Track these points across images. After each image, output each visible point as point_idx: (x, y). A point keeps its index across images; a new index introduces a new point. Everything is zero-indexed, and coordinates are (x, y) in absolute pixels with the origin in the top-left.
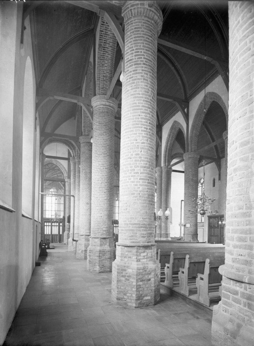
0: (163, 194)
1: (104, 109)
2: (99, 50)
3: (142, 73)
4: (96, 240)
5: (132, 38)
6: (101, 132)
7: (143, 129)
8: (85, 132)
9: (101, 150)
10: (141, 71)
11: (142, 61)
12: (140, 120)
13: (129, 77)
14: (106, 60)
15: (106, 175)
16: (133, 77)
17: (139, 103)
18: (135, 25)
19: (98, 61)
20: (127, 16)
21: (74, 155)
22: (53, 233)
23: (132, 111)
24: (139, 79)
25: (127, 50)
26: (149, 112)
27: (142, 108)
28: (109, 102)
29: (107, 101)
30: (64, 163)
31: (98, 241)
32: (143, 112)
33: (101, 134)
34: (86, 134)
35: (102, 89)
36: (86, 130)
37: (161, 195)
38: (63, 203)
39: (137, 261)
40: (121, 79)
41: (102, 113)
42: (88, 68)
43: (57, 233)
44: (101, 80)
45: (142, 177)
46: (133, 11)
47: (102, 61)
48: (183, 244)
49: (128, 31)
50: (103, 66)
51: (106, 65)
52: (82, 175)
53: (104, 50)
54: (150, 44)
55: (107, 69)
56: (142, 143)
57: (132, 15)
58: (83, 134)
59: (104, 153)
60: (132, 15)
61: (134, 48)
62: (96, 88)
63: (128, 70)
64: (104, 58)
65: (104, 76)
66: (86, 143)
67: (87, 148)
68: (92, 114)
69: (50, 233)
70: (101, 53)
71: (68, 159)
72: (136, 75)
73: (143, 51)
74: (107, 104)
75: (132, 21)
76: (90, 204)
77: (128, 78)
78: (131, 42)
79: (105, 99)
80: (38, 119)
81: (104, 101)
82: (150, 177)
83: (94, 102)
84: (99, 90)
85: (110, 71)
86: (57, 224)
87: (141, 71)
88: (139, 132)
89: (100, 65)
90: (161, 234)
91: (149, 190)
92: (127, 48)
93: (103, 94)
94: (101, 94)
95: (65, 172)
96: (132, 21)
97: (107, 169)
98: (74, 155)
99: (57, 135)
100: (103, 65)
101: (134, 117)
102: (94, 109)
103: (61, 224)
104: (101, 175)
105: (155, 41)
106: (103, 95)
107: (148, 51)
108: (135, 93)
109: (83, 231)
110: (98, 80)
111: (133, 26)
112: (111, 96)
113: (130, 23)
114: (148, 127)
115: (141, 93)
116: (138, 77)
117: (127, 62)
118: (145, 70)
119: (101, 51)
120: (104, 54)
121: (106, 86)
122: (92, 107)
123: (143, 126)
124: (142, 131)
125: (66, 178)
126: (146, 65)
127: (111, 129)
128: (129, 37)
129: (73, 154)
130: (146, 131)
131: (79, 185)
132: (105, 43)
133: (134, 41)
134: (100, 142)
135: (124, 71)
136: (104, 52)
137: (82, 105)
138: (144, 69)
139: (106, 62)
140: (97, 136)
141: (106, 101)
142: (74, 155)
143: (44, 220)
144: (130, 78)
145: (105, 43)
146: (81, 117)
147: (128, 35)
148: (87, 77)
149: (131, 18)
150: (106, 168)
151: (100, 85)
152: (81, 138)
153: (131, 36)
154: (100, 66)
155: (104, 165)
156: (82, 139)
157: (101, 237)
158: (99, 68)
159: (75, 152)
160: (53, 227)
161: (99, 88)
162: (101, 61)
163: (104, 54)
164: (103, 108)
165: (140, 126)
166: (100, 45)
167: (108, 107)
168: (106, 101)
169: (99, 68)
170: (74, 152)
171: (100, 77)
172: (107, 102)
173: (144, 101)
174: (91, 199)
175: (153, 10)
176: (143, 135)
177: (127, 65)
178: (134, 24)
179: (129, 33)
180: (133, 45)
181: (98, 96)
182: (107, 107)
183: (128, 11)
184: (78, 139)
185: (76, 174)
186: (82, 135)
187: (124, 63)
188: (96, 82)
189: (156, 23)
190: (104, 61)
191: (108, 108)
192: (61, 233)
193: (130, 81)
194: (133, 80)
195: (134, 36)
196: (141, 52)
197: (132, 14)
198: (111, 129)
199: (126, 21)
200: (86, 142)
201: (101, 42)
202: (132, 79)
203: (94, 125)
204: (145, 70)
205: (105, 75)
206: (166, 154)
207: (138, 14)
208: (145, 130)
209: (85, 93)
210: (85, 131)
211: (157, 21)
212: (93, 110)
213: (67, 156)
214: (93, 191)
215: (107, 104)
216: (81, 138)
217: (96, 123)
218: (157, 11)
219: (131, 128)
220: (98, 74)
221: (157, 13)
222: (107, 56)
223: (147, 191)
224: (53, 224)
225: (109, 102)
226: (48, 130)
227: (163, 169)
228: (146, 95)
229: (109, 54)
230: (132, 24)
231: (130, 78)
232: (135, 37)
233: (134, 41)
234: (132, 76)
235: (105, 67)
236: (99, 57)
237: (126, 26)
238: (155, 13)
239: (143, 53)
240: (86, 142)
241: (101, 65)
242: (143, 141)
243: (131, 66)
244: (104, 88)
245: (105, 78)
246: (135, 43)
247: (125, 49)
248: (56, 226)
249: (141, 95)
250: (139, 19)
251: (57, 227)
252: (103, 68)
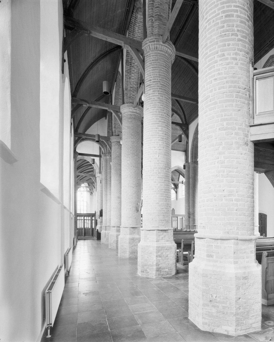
0: (190, 188)
1: (131, 116)
2: (127, 65)
3: (158, 96)
4: (126, 229)
5: (150, 68)
6: (129, 136)
7: (160, 139)
8: (115, 132)
9: (129, 151)
10: (157, 94)
11: (158, 87)
12: (157, 132)
13: (149, 98)
14: (133, 73)
15: (134, 172)
16: (151, 99)
17: (156, 119)
18: (152, 58)
19: (126, 74)
20: (146, 50)
21: (105, 152)
22: (85, 227)
23: (236, 17)
24: (156, 100)
25: (147, 77)
26: (165, 126)
27: (159, 122)
28: (136, 110)
29: (134, 108)
30: (97, 159)
31: (128, 230)
32: (160, 126)
33: (129, 137)
34: (117, 134)
35: (130, 98)
36: (116, 131)
37: (189, 189)
38: (121, 98)
39: (157, 241)
40: (143, 99)
41: (130, 119)
42: (118, 76)
43: (90, 227)
44: (129, 91)
45: (160, 176)
46: (150, 46)
47: (129, 74)
48: (64, 180)
49: (147, 62)
50: (130, 79)
51: (132, 78)
52: (113, 171)
53: (130, 65)
54: (165, 73)
55: (134, 81)
56: (159, 150)
57: (150, 49)
58: (114, 134)
59: (132, 153)
60: (150, 49)
61: (152, 76)
62: (125, 97)
63: (148, 93)
64: (131, 72)
65: (131, 87)
66: (116, 143)
67: (117, 147)
68: (121, 120)
69: (82, 227)
70: (128, 67)
71: (100, 156)
72: (154, 97)
73: (159, 78)
74: (134, 111)
75: (150, 54)
76: (120, 198)
77: (148, 99)
78: (150, 71)
79: (132, 107)
80: (72, 124)
81: (131, 109)
82: (166, 176)
83: (123, 109)
84: (127, 99)
85: (136, 83)
86: (90, 218)
87: (157, 94)
88: (157, 141)
89: (127, 77)
90: (189, 226)
91: (165, 186)
92: (147, 76)
93: (131, 103)
94: (129, 103)
95: (97, 167)
96: (150, 54)
97: (134, 167)
98: (106, 152)
99: (88, 135)
100: (130, 78)
101: (153, 130)
102: (123, 116)
103: (93, 218)
104: (130, 172)
105: (169, 70)
106: (130, 104)
107: (164, 78)
108: (153, 111)
109: (114, 222)
110: (125, 90)
111: (151, 58)
112: (137, 104)
113: (148, 56)
114: (164, 137)
115: (158, 111)
116: (156, 99)
117: (147, 86)
118: (161, 94)
119: (129, 66)
120: (131, 68)
121: (132, 96)
122: (121, 113)
123: (160, 137)
124: (159, 140)
125: (98, 173)
126: (162, 89)
127: (138, 132)
128: (148, 67)
129: (105, 152)
130: (162, 140)
131: (111, 181)
132: (131, 59)
133: (152, 70)
134: (128, 144)
135: (145, 93)
136: (131, 66)
137: (112, 111)
138: (160, 92)
139: (133, 75)
140: (126, 139)
141: (133, 109)
142: (106, 152)
143: (77, 215)
144: (149, 99)
145: (131, 59)
146: (112, 120)
147: (148, 65)
148: (116, 84)
149: (149, 52)
150: (133, 167)
151: (127, 94)
152: (112, 138)
153: (150, 66)
154: (127, 79)
155: (132, 164)
156: (113, 139)
157: (130, 227)
158: (126, 80)
159: (107, 150)
160: (85, 221)
161: (127, 97)
162: (129, 74)
163: (131, 68)
164: (131, 114)
165: (157, 136)
166: (127, 61)
167: (135, 114)
168: (133, 109)
169: (126, 80)
170: (105, 150)
171: (127, 88)
172: (135, 109)
173: (160, 117)
174: (121, 194)
175: (167, 45)
176: (160, 143)
177: (147, 89)
178: (151, 57)
179: (148, 64)
180: (152, 74)
181: (126, 105)
182: (134, 113)
183: (147, 46)
184: (109, 139)
185: (108, 170)
186: (113, 135)
187: (145, 86)
188: (125, 92)
189: (169, 55)
190: (130, 74)
191: (135, 115)
192: (93, 227)
193: (149, 101)
194: (151, 101)
195: (152, 66)
196: (158, 79)
197: (150, 48)
198: (138, 132)
199: (146, 54)
200: (117, 142)
201: (128, 58)
202: (150, 100)
203: (123, 129)
204: (161, 94)
205: (132, 86)
206: (193, 151)
207: (154, 49)
208: (162, 139)
209: (115, 98)
210: (115, 131)
211: (170, 54)
212: (122, 116)
213: (98, 154)
214: (123, 187)
215: (134, 111)
216: (112, 138)
217: (125, 127)
218: (170, 46)
219: (150, 138)
220: (126, 85)
221: (170, 47)
222: (133, 70)
223: (164, 187)
224: (85, 218)
225: (136, 110)
226: (80, 130)
227: (190, 164)
228: (162, 112)
229: (135, 69)
230: (150, 56)
231: (149, 99)
232: (152, 68)
233: (152, 70)
234: (150, 98)
235: (132, 79)
236: (127, 71)
237: (145, 58)
238: (168, 48)
239: (159, 80)
240: (117, 142)
241: (128, 78)
242: (160, 148)
243: (150, 90)
244: (131, 98)
245: (132, 89)
246: (152, 72)
247: (145, 76)
248: (89, 220)
249: (158, 113)
250: (155, 53)
251: (90, 221)
252: (130, 80)
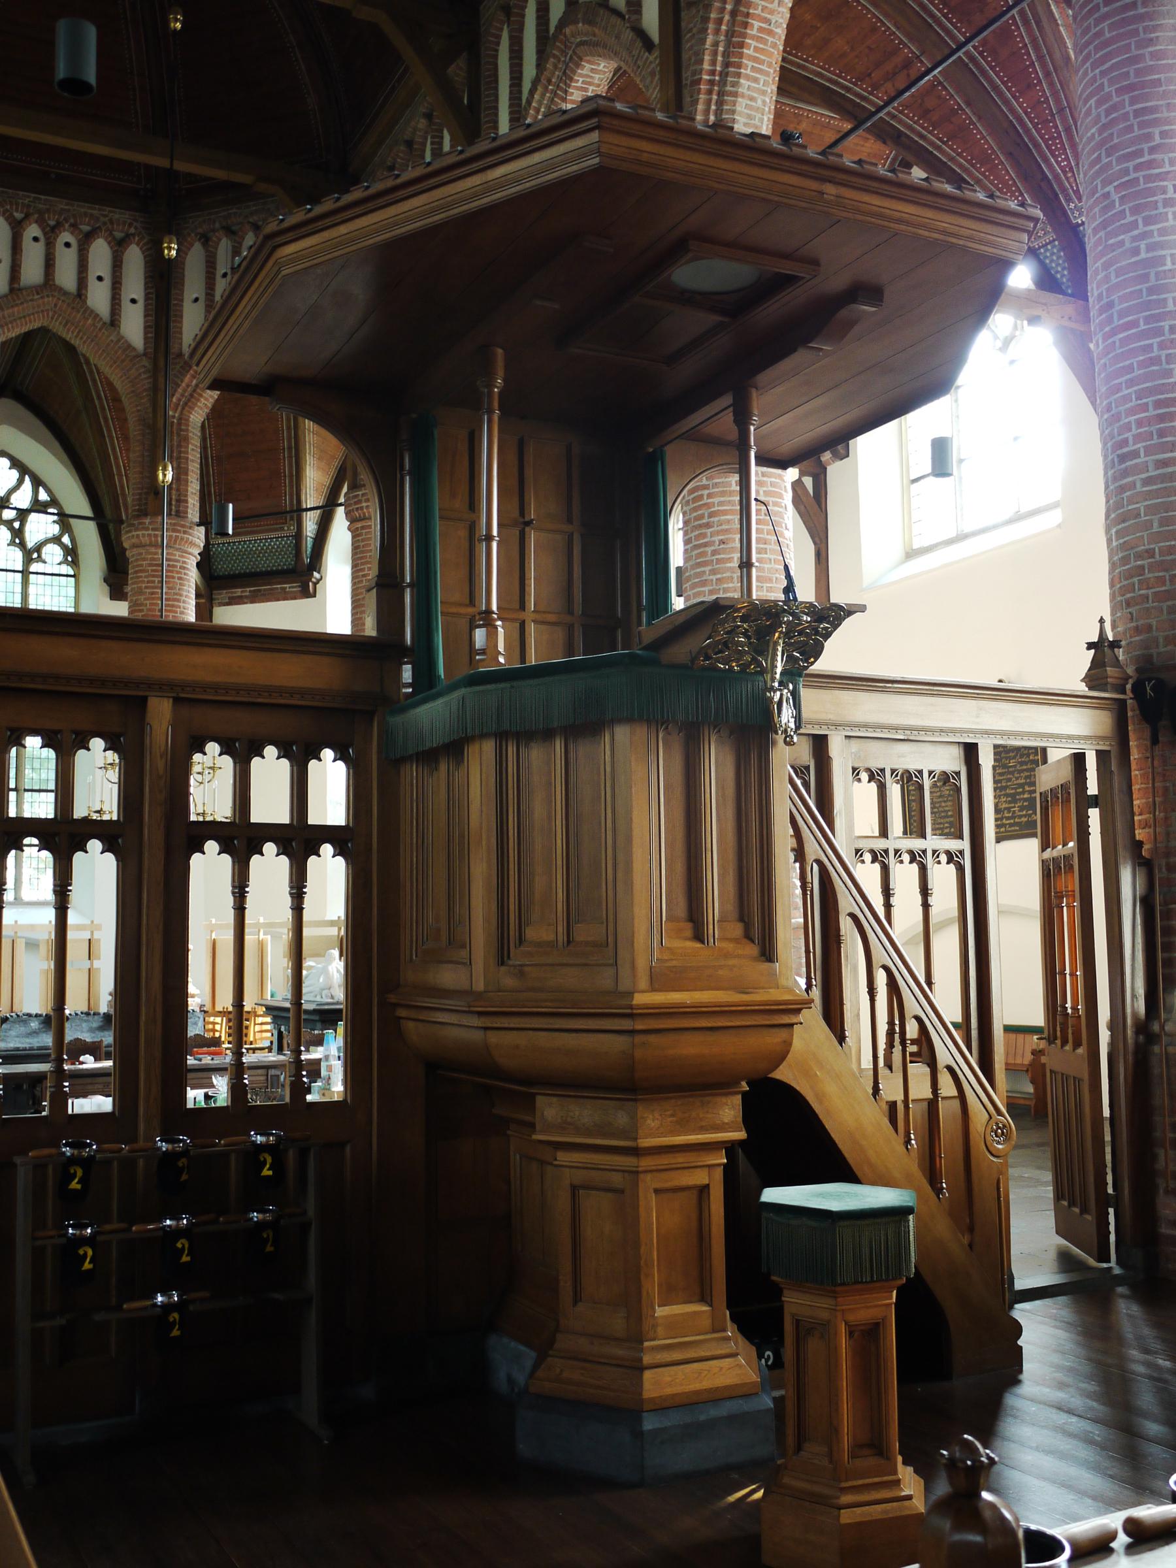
160: (209, 870)
248: (299, 840)
